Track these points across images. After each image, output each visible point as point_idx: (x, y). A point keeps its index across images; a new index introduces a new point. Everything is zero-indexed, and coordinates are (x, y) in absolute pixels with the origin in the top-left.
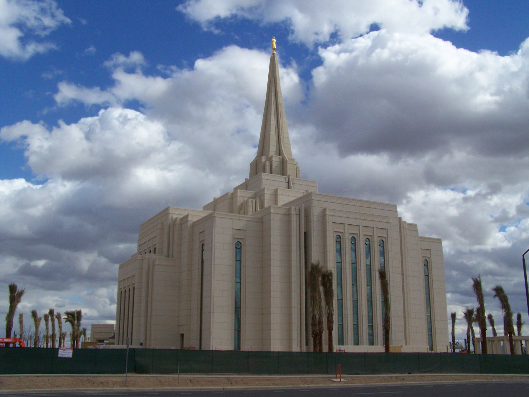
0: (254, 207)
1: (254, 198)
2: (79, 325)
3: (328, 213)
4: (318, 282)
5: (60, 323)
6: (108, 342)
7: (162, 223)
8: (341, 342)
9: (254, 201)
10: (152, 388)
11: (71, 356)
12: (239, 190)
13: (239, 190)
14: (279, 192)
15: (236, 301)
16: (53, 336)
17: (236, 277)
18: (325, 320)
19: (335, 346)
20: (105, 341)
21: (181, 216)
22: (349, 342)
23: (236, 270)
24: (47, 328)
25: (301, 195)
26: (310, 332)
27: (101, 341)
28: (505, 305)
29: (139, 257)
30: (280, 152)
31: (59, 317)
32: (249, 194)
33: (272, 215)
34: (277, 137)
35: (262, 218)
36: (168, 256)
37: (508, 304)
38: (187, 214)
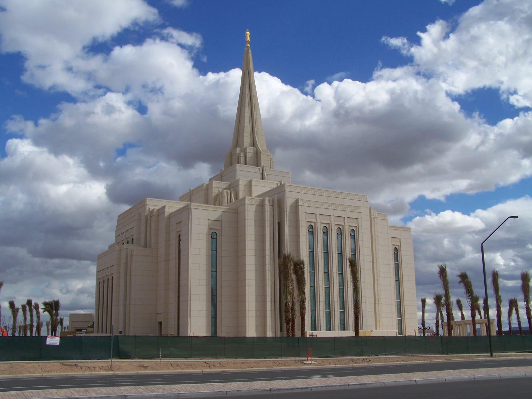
0: (229, 198)
1: (229, 188)
2: (57, 314)
3: (300, 203)
4: (289, 271)
5: (38, 313)
6: (85, 331)
7: (140, 214)
8: (314, 327)
9: (229, 192)
10: (136, 372)
11: (58, 344)
12: (214, 182)
13: (214, 182)
14: (253, 183)
15: (212, 289)
16: (32, 326)
17: (212, 267)
18: (297, 307)
19: (308, 331)
20: (83, 331)
21: (158, 208)
22: (322, 327)
24: (25, 319)
25: (274, 186)
26: (284, 318)
27: (80, 330)
28: (469, 291)
29: (117, 247)
30: (254, 143)
31: (37, 307)
32: (225, 184)
33: (246, 205)
34: (251, 129)
36: (146, 246)
37: (471, 290)
38: (163, 205)
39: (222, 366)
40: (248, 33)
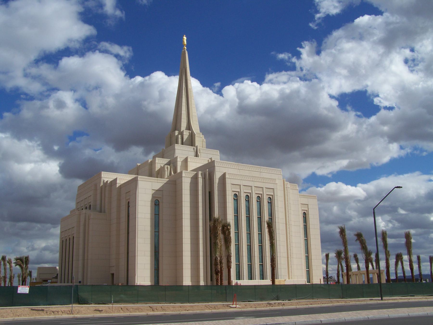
0: (169, 172)
4: (217, 232)
5: (11, 267)
6: (50, 281)
8: (239, 277)
11: (28, 292)
14: (189, 160)
17: (155, 228)
18: (224, 261)
20: (49, 281)
23: (155, 222)
25: (206, 162)
27: (46, 281)
28: (364, 247)
31: (10, 262)
35: (175, 181)
38: (115, 178)
39: (164, 310)
40: (185, 38)
